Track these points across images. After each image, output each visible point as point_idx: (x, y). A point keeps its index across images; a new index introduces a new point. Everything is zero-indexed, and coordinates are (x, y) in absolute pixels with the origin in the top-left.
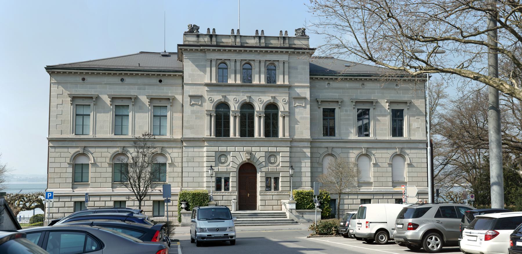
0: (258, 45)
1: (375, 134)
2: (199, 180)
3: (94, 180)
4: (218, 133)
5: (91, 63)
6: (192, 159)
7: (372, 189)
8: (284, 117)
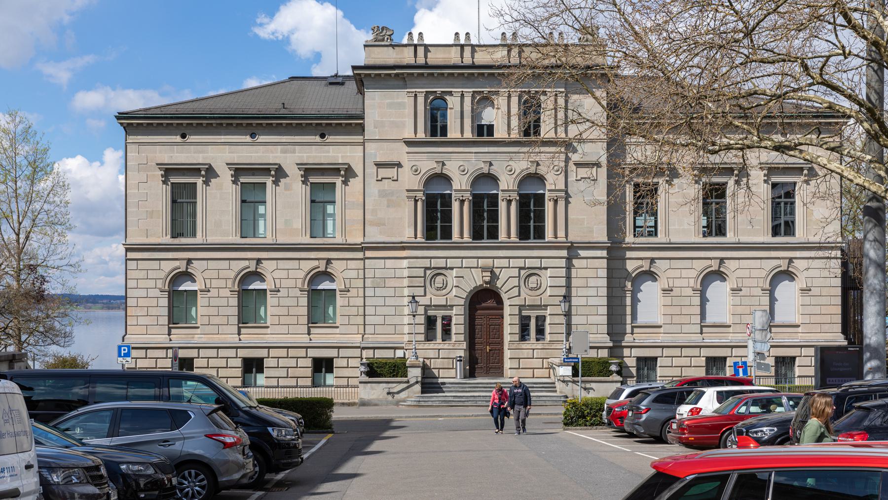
0: (506, 62)
1: (736, 233)
2: (396, 320)
3: (205, 320)
4: (430, 232)
5: (182, 106)
6: (382, 282)
7: (660, 338)
8: (556, 202)
